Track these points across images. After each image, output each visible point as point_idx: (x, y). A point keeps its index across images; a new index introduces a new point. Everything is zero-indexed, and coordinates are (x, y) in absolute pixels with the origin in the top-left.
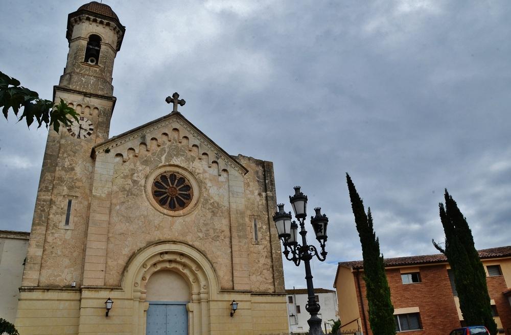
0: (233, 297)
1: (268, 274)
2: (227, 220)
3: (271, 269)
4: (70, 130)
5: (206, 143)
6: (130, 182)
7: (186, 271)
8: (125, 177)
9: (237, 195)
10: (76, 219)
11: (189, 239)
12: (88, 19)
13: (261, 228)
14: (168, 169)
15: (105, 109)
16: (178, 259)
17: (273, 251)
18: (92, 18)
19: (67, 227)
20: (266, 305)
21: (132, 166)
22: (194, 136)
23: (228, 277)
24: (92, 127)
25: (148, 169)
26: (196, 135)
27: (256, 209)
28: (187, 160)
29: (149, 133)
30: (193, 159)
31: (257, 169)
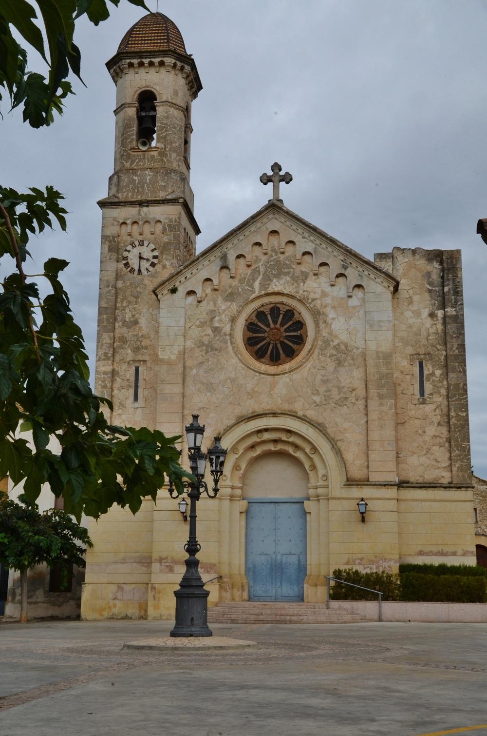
0: (366, 492)
1: (441, 454)
2: (362, 370)
3: (447, 445)
4: (127, 265)
5: (324, 246)
6: (209, 331)
7: (299, 454)
8: (202, 325)
9: (380, 326)
10: (146, 392)
11: (299, 407)
12: (131, 65)
13: (433, 374)
14: (266, 300)
15: (171, 220)
16: (284, 438)
17: (452, 414)
18: (135, 61)
19: (136, 405)
20: (433, 504)
21: (211, 307)
22: (304, 238)
23: (360, 462)
24: (156, 253)
25: (234, 307)
26: (306, 235)
27: (424, 341)
28: (295, 279)
29: (231, 248)
30: (305, 277)
31: (429, 268)
